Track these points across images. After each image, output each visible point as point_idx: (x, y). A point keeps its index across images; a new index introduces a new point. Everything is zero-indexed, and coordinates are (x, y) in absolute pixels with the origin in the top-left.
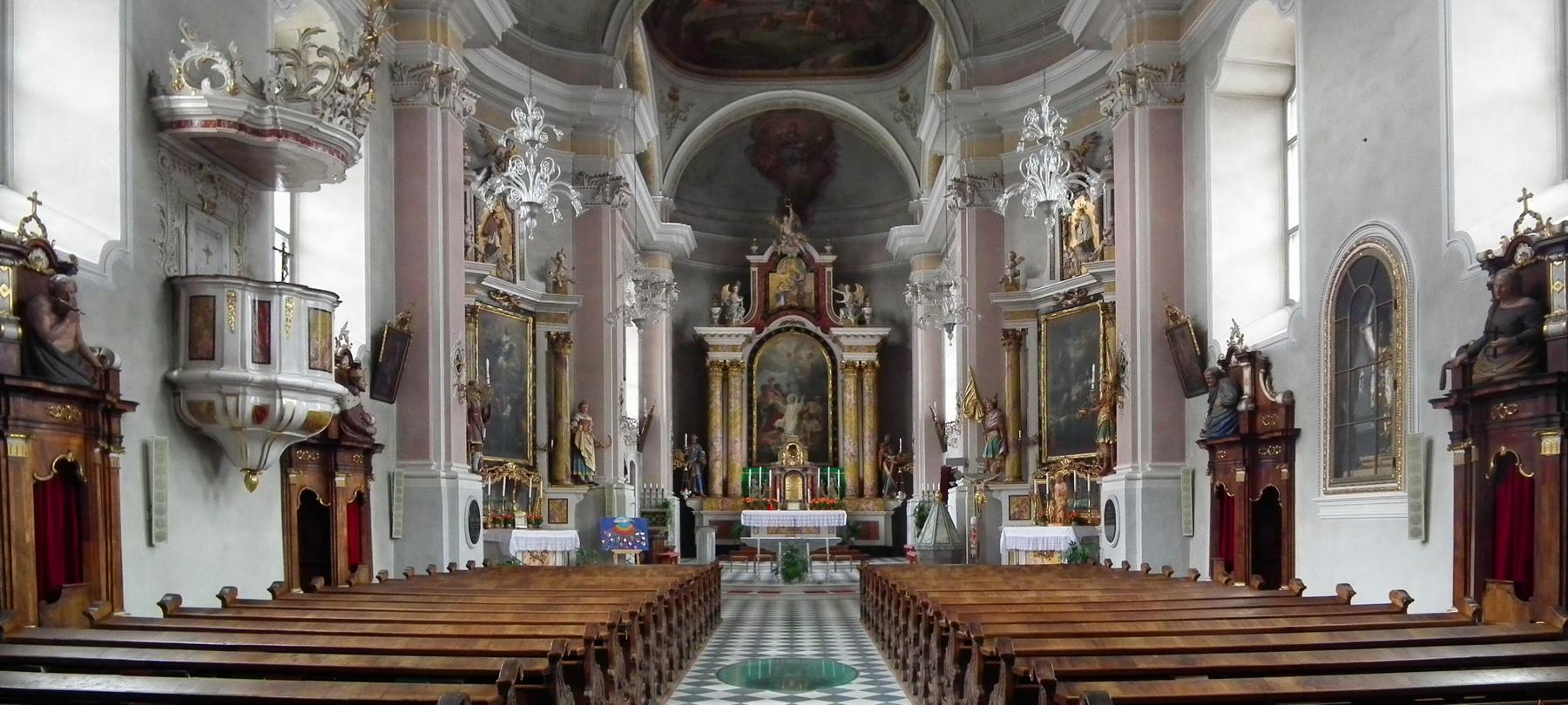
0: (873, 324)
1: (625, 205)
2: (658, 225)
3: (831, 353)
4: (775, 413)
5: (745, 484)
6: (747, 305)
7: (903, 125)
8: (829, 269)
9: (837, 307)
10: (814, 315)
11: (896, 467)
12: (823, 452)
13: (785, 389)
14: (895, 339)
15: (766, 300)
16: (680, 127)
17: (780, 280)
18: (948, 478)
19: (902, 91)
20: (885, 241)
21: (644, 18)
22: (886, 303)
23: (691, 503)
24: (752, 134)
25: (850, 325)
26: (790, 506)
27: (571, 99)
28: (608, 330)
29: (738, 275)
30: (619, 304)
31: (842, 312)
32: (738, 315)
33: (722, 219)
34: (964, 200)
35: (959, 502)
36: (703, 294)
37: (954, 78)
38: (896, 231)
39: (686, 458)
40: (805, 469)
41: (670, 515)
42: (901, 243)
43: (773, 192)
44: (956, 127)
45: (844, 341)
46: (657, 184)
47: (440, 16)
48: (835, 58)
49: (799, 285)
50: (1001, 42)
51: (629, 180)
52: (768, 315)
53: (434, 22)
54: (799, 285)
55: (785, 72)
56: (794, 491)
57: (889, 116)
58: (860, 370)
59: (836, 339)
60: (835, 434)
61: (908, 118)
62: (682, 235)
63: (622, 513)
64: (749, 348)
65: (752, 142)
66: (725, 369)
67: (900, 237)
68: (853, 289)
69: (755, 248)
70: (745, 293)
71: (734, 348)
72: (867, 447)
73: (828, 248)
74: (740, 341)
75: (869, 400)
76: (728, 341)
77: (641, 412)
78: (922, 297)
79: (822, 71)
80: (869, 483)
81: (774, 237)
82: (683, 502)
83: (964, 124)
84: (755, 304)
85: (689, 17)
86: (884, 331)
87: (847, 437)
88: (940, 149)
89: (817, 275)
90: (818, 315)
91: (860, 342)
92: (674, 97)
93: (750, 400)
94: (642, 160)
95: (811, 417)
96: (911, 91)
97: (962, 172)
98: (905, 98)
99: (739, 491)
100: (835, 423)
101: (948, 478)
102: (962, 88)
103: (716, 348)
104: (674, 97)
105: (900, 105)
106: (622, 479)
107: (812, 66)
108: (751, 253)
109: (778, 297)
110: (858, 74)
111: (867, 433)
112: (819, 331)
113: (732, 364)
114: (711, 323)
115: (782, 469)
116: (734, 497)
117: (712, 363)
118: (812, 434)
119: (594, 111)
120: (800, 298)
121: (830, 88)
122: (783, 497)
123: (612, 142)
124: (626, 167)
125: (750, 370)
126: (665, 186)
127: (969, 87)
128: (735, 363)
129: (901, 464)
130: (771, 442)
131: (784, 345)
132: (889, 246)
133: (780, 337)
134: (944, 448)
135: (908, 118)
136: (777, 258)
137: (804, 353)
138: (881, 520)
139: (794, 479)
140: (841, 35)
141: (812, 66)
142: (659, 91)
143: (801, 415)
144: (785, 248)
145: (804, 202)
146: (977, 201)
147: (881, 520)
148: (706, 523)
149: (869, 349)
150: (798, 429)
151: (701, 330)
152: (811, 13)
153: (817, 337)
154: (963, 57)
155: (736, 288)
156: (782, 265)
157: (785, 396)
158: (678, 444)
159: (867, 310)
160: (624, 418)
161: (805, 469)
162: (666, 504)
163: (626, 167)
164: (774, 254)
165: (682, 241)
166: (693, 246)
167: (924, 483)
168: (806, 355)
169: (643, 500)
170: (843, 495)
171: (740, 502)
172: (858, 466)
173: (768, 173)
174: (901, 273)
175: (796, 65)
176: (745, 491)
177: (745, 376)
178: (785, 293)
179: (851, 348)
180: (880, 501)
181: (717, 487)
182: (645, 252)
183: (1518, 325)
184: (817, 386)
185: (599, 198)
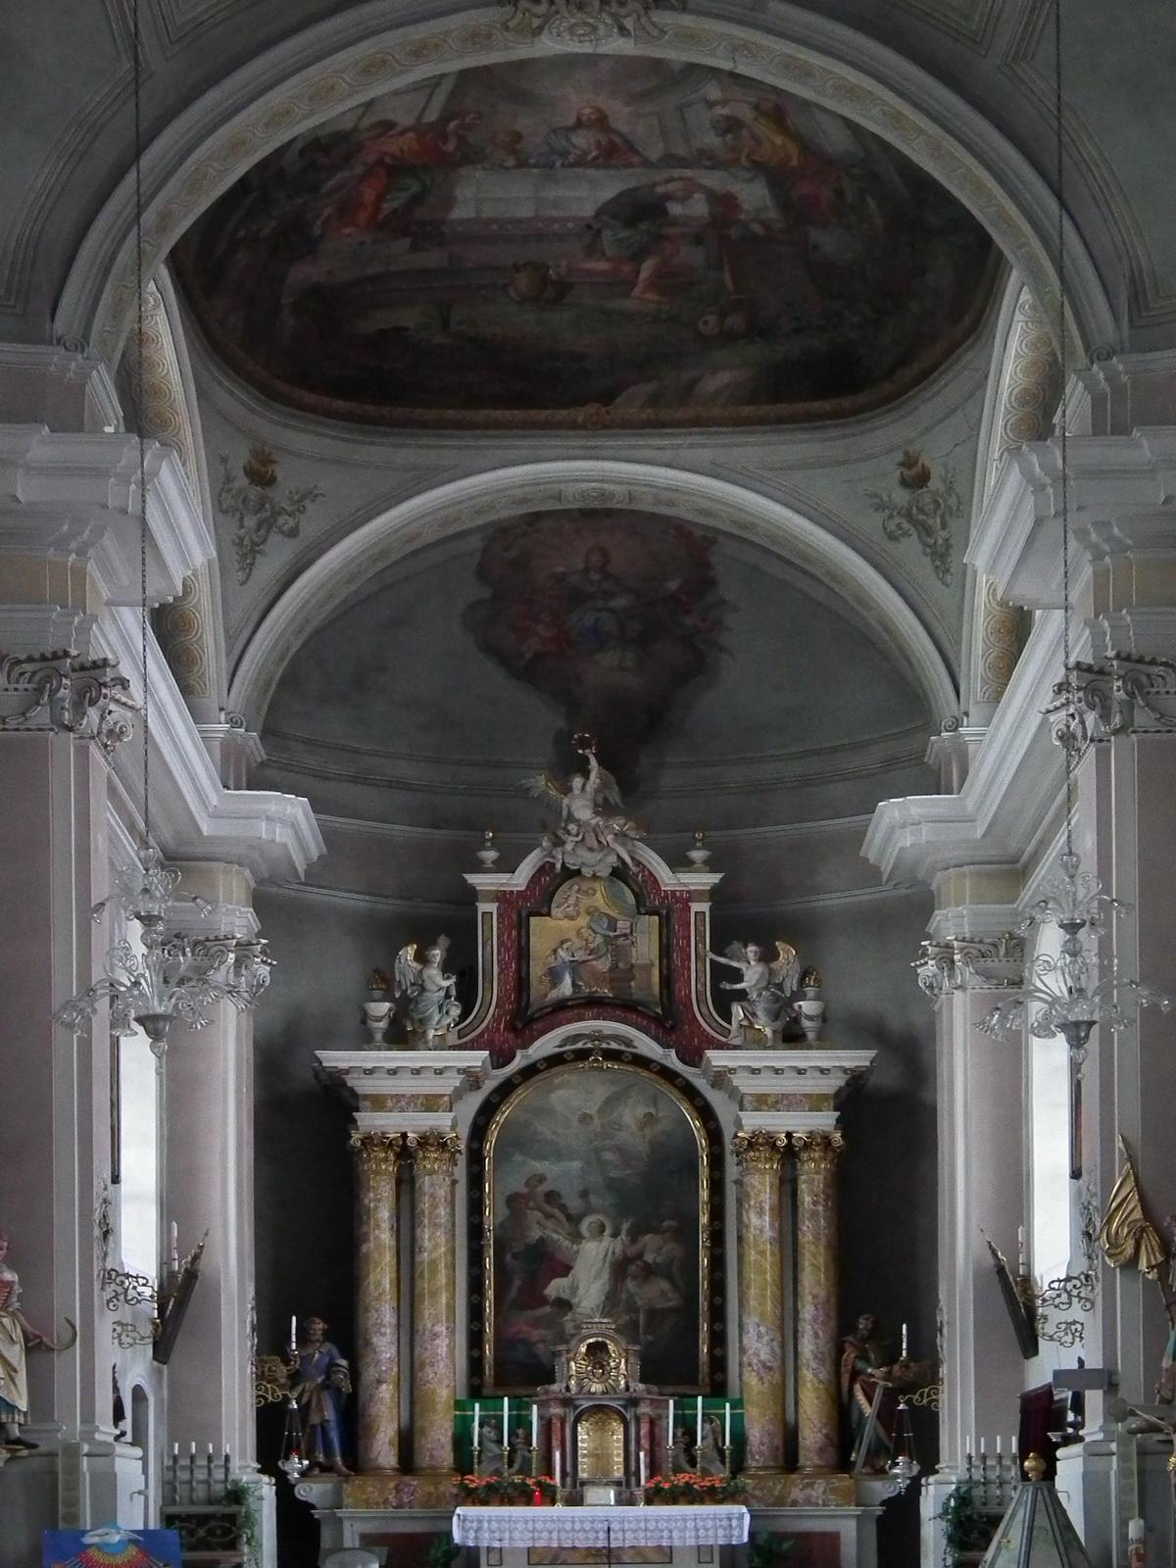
0: (824, 1041)
1: (116, 734)
2: (214, 795)
3: (706, 1113)
4: (547, 1262)
5: (461, 1440)
6: (466, 995)
7: (910, 549)
8: (704, 907)
9: (723, 1003)
10: (658, 1021)
11: (890, 1397)
12: (681, 1353)
13: (574, 1203)
14: (889, 1078)
15: (522, 984)
16: (278, 555)
17: (561, 935)
18: (1043, 1423)
19: (909, 462)
20: (859, 837)
21: (174, 261)
22: (860, 986)
23: (311, 1491)
24: (482, 573)
25: (760, 1043)
26: (592, 1494)
28: (65, 1047)
29: (448, 923)
30: (97, 974)
31: (738, 1011)
32: (441, 1019)
33: (393, 784)
34: (1105, 717)
35: (1092, 1484)
36: (336, 971)
37: (1075, 405)
38: (891, 810)
39: (295, 1378)
40: (633, 1402)
41: (250, 1520)
42: (906, 840)
43: (544, 718)
44: (1081, 534)
45: (744, 1084)
46: (214, 692)
49: (616, 945)
51: (126, 670)
52: (525, 1018)
54: (616, 945)
55: (580, 414)
56: (600, 1456)
57: (871, 524)
58: (789, 1154)
59: (720, 1079)
60: (718, 1314)
62: (284, 822)
63: (106, 1513)
64: (474, 1102)
65: (486, 593)
66: (405, 1153)
67: (903, 826)
68: (768, 956)
69: (490, 855)
70: (464, 971)
71: (430, 1103)
72: (807, 1346)
73: (698, 855)
74: (450, 1084)
75: (814, 1232)
76: (414, 1084)
77: (164, 1262)
78: (965, 973)
79: (680, 414)
80: (812, 1435)
81: (544, 827)
82: (284, 1490)
83: (1102, 526)
84: (491, 993)
85: (304, 273)
86: (858, 1058)
87: (751, 1321)
88: (1026, 591)
89: (665, 924)
90: (668, 1018)
91: (788, 1085)
92: (261, 475)
93: (475, 1232)
94: (169, 626)
95: (649, 1272)
96: (933, 459)
97: (1097, 645)
98: (916, 479)
99: (446, 1457)
100: (718, 1288)
101: (1043, 1423)
102: (1098, 429)
103: (379, 1103)
104: (261, 475)
105: (901, 497)
106: (106, 1430)
107: (654, 400)
108: (478, 867)
109: (554, 976)
110: (779, 422)
111: (808, 1312)
112: (672, 1060)
113: (424, 1141)
114: (364, 1039)
115: (567, 1402)
116: (433, 1474)
117: (368, 1141)
118: (653, 1314)
120: (621, 975)
121: (705, 455)
122: (571, 1472)
123: (80, 575)
124: (122, 636)
125: (475, 1157)
126: (236, 700)
127: (1121, 429)
128: (432, 1141)
129: (906, 1388)
130: (535, 1334)
131: (575, 1097)
132: (871, 850)
133: (562, 1075)
134: (1029, 1343)
135: (926, 530)
136: (551, 882)
137: (631, 1114)
138: (848, 1530)
139: (601, 1427)
140: (735, 321)
142: (218, 460)
143: (620, 1269)
144: (572, 854)
145: (628, 741)
146: (1143, 718)
147: (848, 1530)
148: (350, 1538)
149: (815, 1103)
150: (612, 1302)
151: (335, 1058)
152: (648, 267)
153: (667, 1074)
154: (1099, 354)
155: (437, 954)
156: (568, 896)
157: (574, 1220)
158: (271, 1340)
159: (807, 1007)
160: (115, 1276)
161: (633, 1402)
162: (237, 1495)
163: (122, 636)
164: (543, 870)
165: (282, 835)
166: (315, 848)
167: (968, 1435)
168: (637, 1118)
169: (169, 1487)
170: (738, 1467)
171: (450, 1486)
172: (784, 1391)
173: (528, 672)
174: (906, 913)
175: (607, 398)
176: (464, 1460)
177: (461, 1171)
178: (575, 967)
179: (762, 1102)
180: (843, 1481)
181: (384, 1450)
182: (181, 860)
183: (709, 1494)
184: (671, 1197)
185: (41, 715)
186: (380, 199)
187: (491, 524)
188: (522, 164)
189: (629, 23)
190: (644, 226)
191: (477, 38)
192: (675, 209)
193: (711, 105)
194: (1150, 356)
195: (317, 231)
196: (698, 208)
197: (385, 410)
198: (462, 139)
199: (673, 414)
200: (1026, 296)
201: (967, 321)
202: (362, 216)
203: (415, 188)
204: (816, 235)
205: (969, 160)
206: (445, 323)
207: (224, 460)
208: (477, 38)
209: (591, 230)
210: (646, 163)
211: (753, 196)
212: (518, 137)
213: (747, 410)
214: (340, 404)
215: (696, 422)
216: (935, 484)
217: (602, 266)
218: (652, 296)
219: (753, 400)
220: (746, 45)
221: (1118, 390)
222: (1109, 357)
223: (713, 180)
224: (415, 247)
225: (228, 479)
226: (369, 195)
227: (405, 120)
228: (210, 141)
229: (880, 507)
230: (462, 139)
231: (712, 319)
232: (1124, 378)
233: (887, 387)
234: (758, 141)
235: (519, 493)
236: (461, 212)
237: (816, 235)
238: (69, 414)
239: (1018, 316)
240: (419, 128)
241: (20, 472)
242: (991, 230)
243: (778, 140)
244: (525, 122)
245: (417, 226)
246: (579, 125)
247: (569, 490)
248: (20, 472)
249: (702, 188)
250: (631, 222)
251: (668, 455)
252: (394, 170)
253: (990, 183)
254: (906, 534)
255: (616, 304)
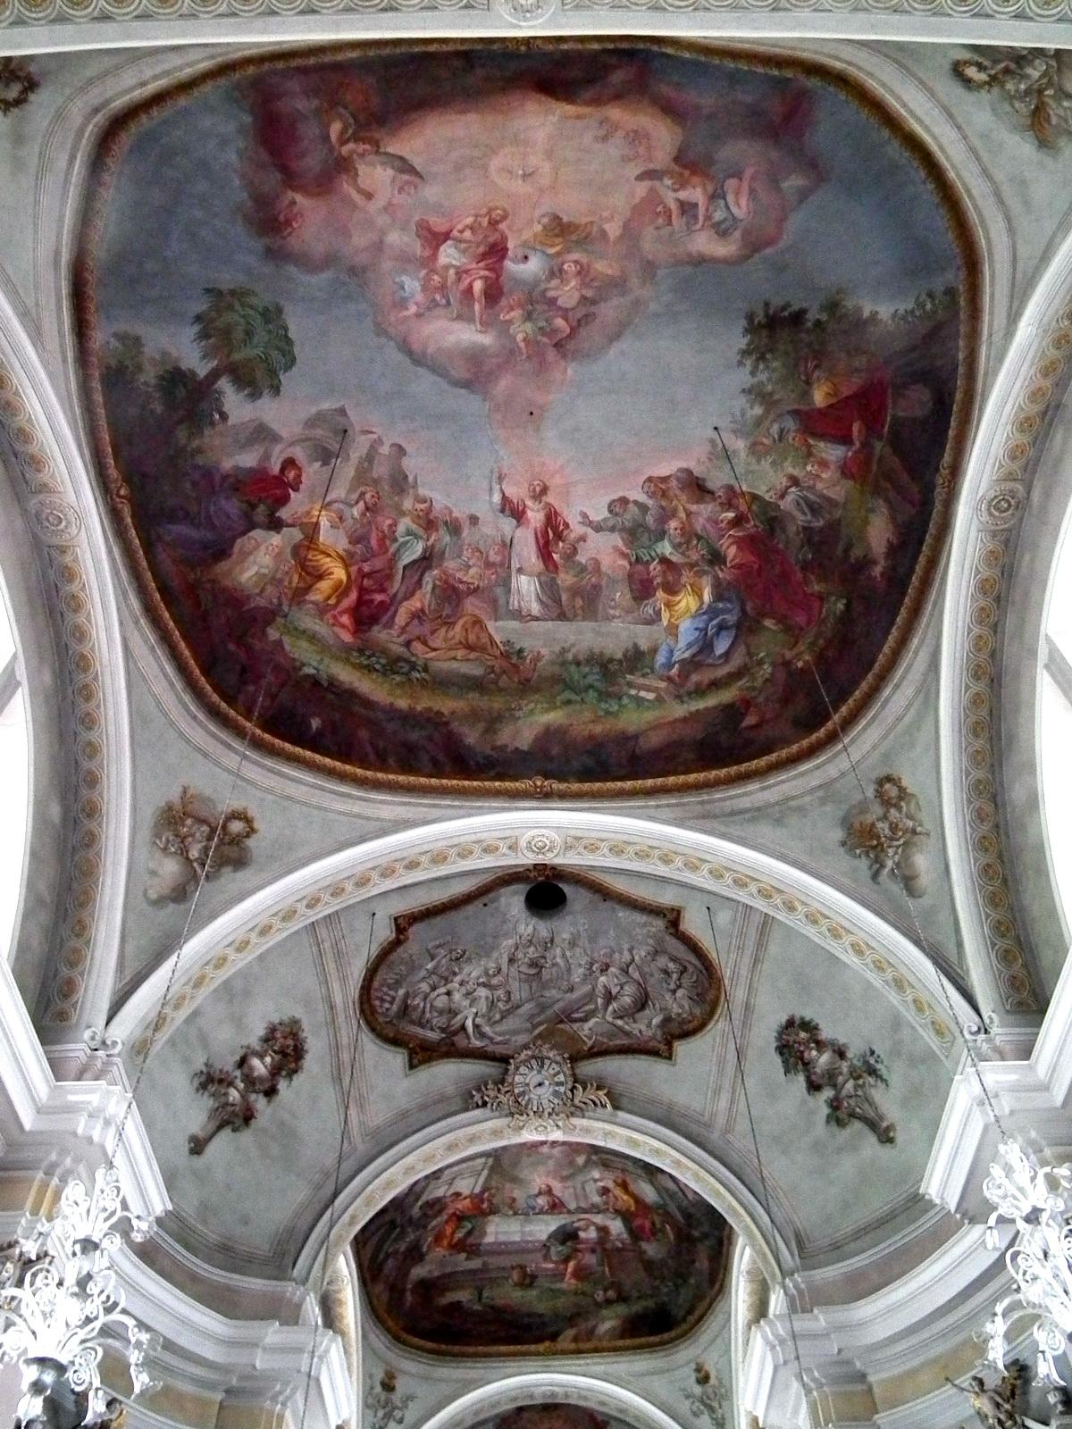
19: (698, 1369)
27: (231, 1343)
37: (777, 1302)
47: (55, 1181)
48: (606, 1326)
50: (837, 1250)
53: (44, 1186)
55: (541, 1347)
57: (685, 1407)
61: (711, 1409)
85: (418, 1272)
92: (388, 1387)
104: (388, 1387)
105: (697, 1390)
107: (576, 1339)
119: (261, 1362)
121: (600, 1369)
135: (711, 1409)
140: (611, 1294)
141: (576, 1339)
152: (572, 1264)
175: (554, 1337)
186: (453, 1233)
187: (497, 1416)
188: (515, 1214)
189: (560, 1123)
190: (569, 1244)
191: (496, 1133)
192: (582, 1235)
193: (596, 1181)
194: (813, 1272)
195: (425, 1249)
196: (592, 1234)
197: (450, 1348)
198: (489, 1201)
199: (587, 1346)
200: (748, 1251)
201: (717, 1286)
202: (445, 1242)
203: (469, 1226)
204: (645, 1246)
205: (712, 1180)
206: (480, 1298)
207: (371, 1376)
208: (496, 1133)
209: (545, 1246)
210: (569, 1212)
211: (616, 1226)
212: (514, 1200)
213: (620, 1343)
214: (430, 1345)
215: (596, 1350)
216: (713, 1381)
217: (551, 1266)
218: (573, 1281)
219: (622, 1336)
220: (610, 1133)
221: (800, 1292)
222: (792, 1274)
223: (599, 1219)
224: (467, 1259)
225: (372, 1388)
226: (449, 1230)
227: (466, 1192)
228: (377, 1181)
229: (687, 1397)
230: (489, 1201)
231: (601, 1293)
232: (803, 1286)
233: (684, 1326)
234: (616, 1198)
235: (513, 1393)
236: (489, 1239)
237: (645, 1246)
238: (289, 1315)
239: (741, 1279)
240: (471, 1196)
241: (259, 1351)
242: (726, 1216)
243: (625, 1197)
244: (517, 1193)
245: (468, 1247)
246: (540, 1193)
247: (538, 1391)
248: (259, 1351)
249: (594, 1223)
250: (563, 1243)
251: (583, 1369)
252: (459, 1218)
253: (722, 1190)
254: (702, 1413)
255: (558, 1286)
